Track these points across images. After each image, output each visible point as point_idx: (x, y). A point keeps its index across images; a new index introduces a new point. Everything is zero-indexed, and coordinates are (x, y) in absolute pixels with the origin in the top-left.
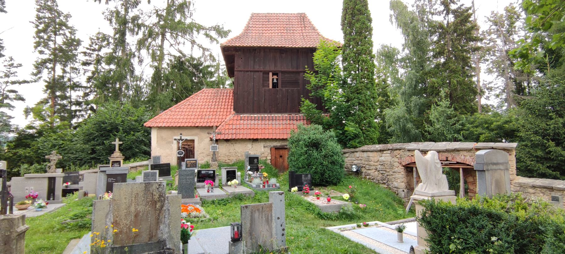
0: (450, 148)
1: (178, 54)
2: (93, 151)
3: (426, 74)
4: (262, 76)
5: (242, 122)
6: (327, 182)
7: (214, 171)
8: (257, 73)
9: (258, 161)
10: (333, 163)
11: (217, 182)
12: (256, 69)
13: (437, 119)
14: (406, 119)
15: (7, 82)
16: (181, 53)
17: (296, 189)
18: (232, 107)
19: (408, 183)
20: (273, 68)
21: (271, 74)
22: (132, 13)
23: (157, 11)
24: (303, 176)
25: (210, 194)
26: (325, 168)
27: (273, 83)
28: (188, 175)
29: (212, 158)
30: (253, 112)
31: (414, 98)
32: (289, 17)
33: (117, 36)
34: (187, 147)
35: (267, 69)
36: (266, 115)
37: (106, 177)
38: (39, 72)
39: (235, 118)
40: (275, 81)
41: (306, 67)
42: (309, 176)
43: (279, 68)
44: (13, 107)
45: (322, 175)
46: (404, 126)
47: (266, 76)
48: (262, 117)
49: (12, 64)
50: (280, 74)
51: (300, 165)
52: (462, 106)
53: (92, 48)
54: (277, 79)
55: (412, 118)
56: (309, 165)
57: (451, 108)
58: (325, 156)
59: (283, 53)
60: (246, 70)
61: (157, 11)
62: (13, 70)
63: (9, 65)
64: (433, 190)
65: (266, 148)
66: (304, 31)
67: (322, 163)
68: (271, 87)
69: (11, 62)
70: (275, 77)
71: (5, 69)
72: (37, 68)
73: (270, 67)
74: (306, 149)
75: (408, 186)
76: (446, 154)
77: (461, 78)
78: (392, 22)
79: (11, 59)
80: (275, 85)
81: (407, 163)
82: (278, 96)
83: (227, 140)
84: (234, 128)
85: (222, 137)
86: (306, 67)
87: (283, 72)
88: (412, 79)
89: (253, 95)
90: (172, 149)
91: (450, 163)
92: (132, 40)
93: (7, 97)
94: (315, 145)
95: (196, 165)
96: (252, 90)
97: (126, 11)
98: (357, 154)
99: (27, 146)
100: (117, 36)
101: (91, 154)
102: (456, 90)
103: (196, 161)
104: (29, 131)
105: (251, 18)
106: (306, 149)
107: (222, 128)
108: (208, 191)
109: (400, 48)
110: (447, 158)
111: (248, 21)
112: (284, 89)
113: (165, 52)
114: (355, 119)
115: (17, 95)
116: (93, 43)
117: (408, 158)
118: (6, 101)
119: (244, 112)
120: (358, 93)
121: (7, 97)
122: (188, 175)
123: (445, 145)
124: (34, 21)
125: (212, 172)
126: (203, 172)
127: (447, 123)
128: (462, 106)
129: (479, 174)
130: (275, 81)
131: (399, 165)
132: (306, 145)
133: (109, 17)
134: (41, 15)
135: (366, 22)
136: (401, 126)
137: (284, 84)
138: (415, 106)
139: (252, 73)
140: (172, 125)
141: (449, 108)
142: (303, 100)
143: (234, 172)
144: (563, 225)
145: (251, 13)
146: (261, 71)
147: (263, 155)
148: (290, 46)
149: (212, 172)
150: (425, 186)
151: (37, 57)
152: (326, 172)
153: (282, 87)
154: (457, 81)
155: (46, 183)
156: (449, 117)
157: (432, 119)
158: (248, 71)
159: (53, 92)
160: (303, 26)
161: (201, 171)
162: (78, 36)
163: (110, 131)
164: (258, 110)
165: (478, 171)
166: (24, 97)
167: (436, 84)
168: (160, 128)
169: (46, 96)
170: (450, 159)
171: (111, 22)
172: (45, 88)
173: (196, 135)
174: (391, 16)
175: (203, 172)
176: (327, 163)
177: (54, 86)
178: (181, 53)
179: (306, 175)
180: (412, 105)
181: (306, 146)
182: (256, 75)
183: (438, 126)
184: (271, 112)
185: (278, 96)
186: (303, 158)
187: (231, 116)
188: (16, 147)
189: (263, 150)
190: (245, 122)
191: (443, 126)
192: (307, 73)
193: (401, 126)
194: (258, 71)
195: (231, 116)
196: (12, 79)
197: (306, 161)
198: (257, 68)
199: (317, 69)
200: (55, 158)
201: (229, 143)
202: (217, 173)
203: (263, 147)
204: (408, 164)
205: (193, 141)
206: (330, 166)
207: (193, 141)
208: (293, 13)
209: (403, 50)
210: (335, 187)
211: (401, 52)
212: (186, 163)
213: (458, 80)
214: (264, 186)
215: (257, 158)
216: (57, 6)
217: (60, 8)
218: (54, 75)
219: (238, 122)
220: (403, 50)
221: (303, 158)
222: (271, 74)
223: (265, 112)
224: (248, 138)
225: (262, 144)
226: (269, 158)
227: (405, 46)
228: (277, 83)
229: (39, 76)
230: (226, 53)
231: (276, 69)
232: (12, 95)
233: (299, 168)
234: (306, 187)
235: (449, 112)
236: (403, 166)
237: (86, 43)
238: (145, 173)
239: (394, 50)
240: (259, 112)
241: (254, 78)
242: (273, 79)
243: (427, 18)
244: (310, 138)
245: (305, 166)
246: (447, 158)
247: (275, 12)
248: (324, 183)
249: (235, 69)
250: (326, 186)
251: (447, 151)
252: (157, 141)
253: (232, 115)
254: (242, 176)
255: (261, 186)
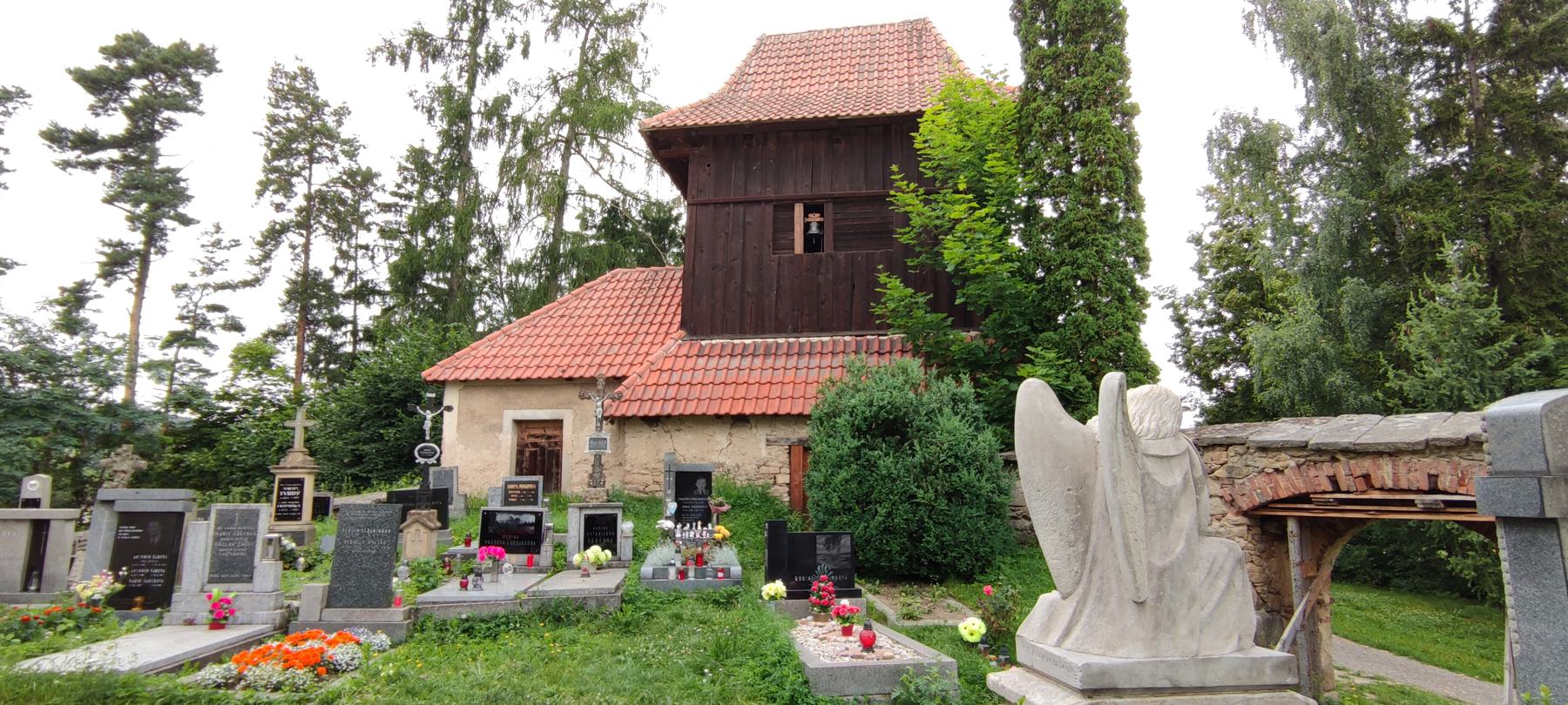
0: (1444, 435)
1: (610, 194)
2: (358, 459)
3: (1394, 199)
4: (769, 219)
5: (701, 362)
6: (935, 566)
7: (539, 516)
8: (756, 209)
9: (709, 487)
10: (954, 495)
11: (546, 554)
12: (752, 196)
13: (1433, 347)
14: (1324, 358)
15: (205, 286)
16: (620, 188)
17: (778, 587)
18: (678, 318)
19: (1268, 582)
20: (804, 191)
21: (799, 209)
22: (487, 90)
23: (555, 82)
24: (821, 540)
25: (471, 594)
26: (922, 512)
27: (808, 238)
28: (371, 525)
29: (591, 476)
30: (742, 333)
31: (1351, 283)
32: (872, 36)
33: (447, 152)
34: (543, 442)
35: (788, 192)
36: (780, 341)
37: (115, 520)
38: (267, 256)
39: (684, 351)
40: (814, 230)
41: (894, 168)
42: (846, 541)
43: (824, 189)
44: (213, 347)
45: (915, 538)
46: (1317, 382)
47: (783, 215)
48: (768, 346)
49: (219, 242)
50: (829, 208)
51: (836, 500)
52: (1543, 304)
53: (402, 191)
54: (821, 225)
55: (1348, 353)
56: (865, 501)
57: (1487, 304)
58: (926, 469)
59: (838, 141)
60: (721, 198)
61: (555, 82)
62: (219, 255)
63: (213, 245)
64: (1110, 647)
65: (775, 449)
66: (915, 70)
67: (915, 496)
68: (799, 247)
69: (216, 236)
70: (815, 218)
71: (202, 255)
72: (261, 244)
73: (797, 185)
74: (856, 443)
75: (1270, 598)
76: (1428, 464)
77: (1534, 207)
78: (1253, 38)
79: (218, 229)
80: (812, 243)
81: (1258, 500)
82: (821, 279)
83: (652, 421)
84: (674, 380)
85: (632, 410)
86: (894, 168)
87: (838, 201)
88: (1339, 221)
89: (743, 276)
90: (499, 447)
91: (1448, 504)
92: (487, 160)
93: (204, 324)
94: (890, 427)
96: (738, 262)
97: (471, 84)
99: (211, 444)
100: (447, 152)
101: (352, 465)
102: (1512, 245)
104: (225, 404)
105: (757, 49)
106: (856, 443)
107: (639, 381)
108: (464, 586)
109: (1293, 121)
110: (1433, 478)
111: (744, 56)
112: (841, 255)
113: (572, 187)
114: (1063, 340)
115: (227, 318)
116: (405, 180)
117: (1261, 481)
118: (199, 334)
119: (712, 332)
120: (1072, 247)
121: (204, 324)
122: (371, 525)
123: (1426, 426)
124: (264, 131)
127: (1473, 363)
128: (1543, 304)
129: (1513, 547)
131: (1224, 509)
132: (859, 429)
133: (427, 103)
134: (282, 113)
136: (1305, 379)
137: (841, 239)
138: (1357, 310)
139: (741, 208)
140: (499, 374)
141: (1480, 305)
142: (883, 278)
143: (611, 522)
144: (1064, 7)
145: (759, 35)
146: (768, 201)
149: (532, 519)
150: (1069, 607)
151: (264, 215)
152: (927, 530)
153: (835, 248)
154: (1517, 215)
155: (23, 536)
156: (1488, 340)
157: (1412, 348)
158: (728, 203)
159: (305, 310)
160: (915, 54)
162: (364, 161)
163: (402, 403)
164: (759, 328)
165: (1510, 522)
166: (243, 323)
167: (1432, 230)
168: (466, 384)
169: (288, 318)
170: (1445, 482)
171: (431, 117)
172: (285, 298)
173: (567, 405)
174: (1249, 18)
175: (500, 518)
176: (931, 494)
177: (308, 292)
178: (620, 188)
179: (834, 539)
180: (1345, 309)
181: (858, 432)
183: (1437, 374)
184: (797, 331)
185: (821, 279)
186: (844, 474)
187: (671, 345)
188: (191, 446)
189: (764, 452)
190: (713, 363)
191: (1460, 372)
192: (899, 189)
193: (1305, 379)
194: (759, 202)
195: (671, 345)
196: (218, 277)
197: (854, 485)
198: (755, 191)
199: (930, 174)
200: (124, 468)
201: (659, 429)
202: (547, 523)
203: (763, 444)
204: (1264, 506)
205: (558, 424)
206: (942, 504)
207: (558, 424)
208: (887, 21)
209: (1305, 126)
210: (961, 588)
211: (1296, 133)
213: (1522, 209)
214: (683, 574)
215: (707, 476)
216: (316, 88)
217: (322, 95)
218: (306, 264)
219: (690, 363)
220: (1305, 126)
221: (844, 474)
222: (799, 209)
223: (779, 330)
224: (711, 412)
225: (760, 435)
226: (784, 478)
227: (1308, 116)
228: (819, 237)
229: (264, 265)
230: (662, 152)
231: (816, 192)
232: (216, 318)
233: (832, 512)
234: (822, 584)
235: (1482, 320)
236: (1245, 514)
237: (389, 177)
238: (220, 513)
239: (1271, 128)
240: (759, 330)
241: (745, 224)
242: (807, 226)
243: (1385, 15)
244: (871, 404)
245: (852, 504)
246: (1433, 478)
247: (834, 27)
248: (924, 572)
250: (925, 581)
251: (1431, 447)
253: (675, 341)
254: (636, 533)
255: (672, 572)
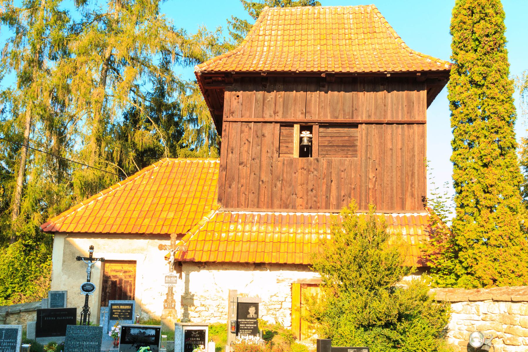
20: (300, 117)
21: (297, 127)
27: (302, 147)
50: (315, 128)
70: (306, 134)
95: (131, 314)
98: (483, 307)
103: (131, 305)
125: (153, 332)
126: (133, 332)
130: (305, 142)
135: (513, 111)
147: (274, 299)
148: (337, 70)
149: (153, 332)
161: (129, 328)
175: (133, 332)
182: (268, 129)
194: (271, 122)
212: (111, 309)
242: (301, 139)
249: (225, 118)
252: (64, 261)
